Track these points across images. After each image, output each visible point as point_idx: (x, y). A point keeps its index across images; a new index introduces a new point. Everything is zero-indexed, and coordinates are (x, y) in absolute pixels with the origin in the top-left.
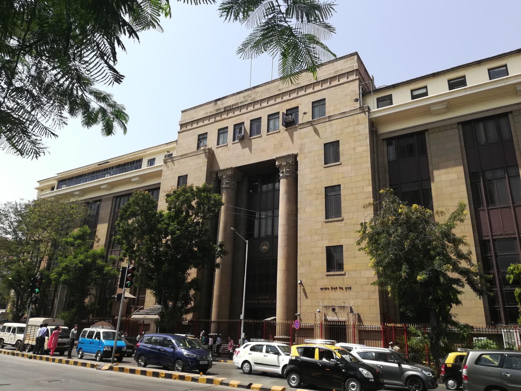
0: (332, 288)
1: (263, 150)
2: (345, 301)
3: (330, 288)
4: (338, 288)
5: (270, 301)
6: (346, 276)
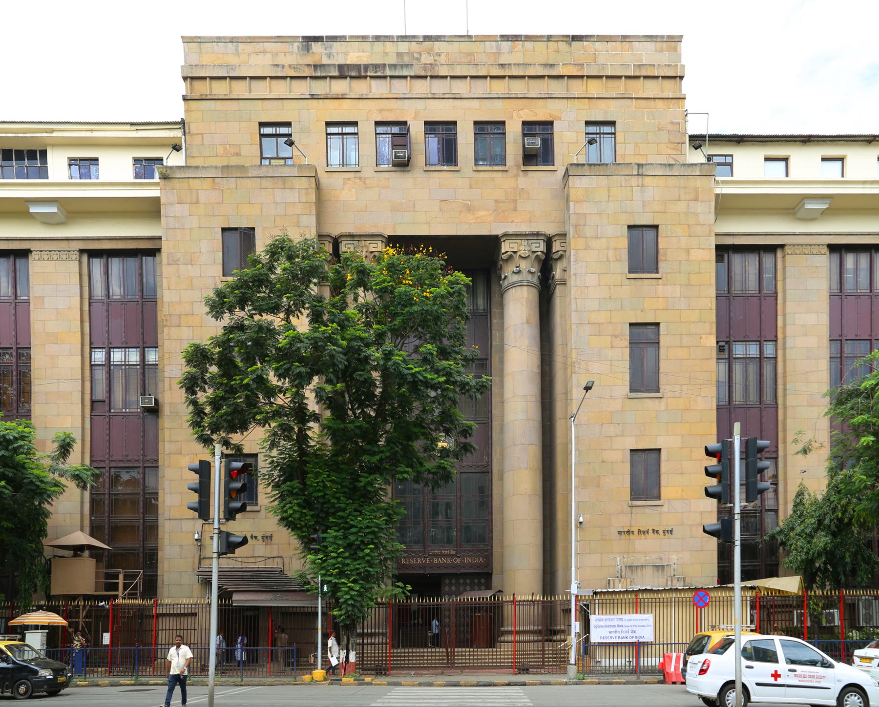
0: (639, 531)
1: (470, 209)
2: (663, 556)
3: (636, 532)
4: (651, 531)
5: (458, 561)
6: (665, 509)
